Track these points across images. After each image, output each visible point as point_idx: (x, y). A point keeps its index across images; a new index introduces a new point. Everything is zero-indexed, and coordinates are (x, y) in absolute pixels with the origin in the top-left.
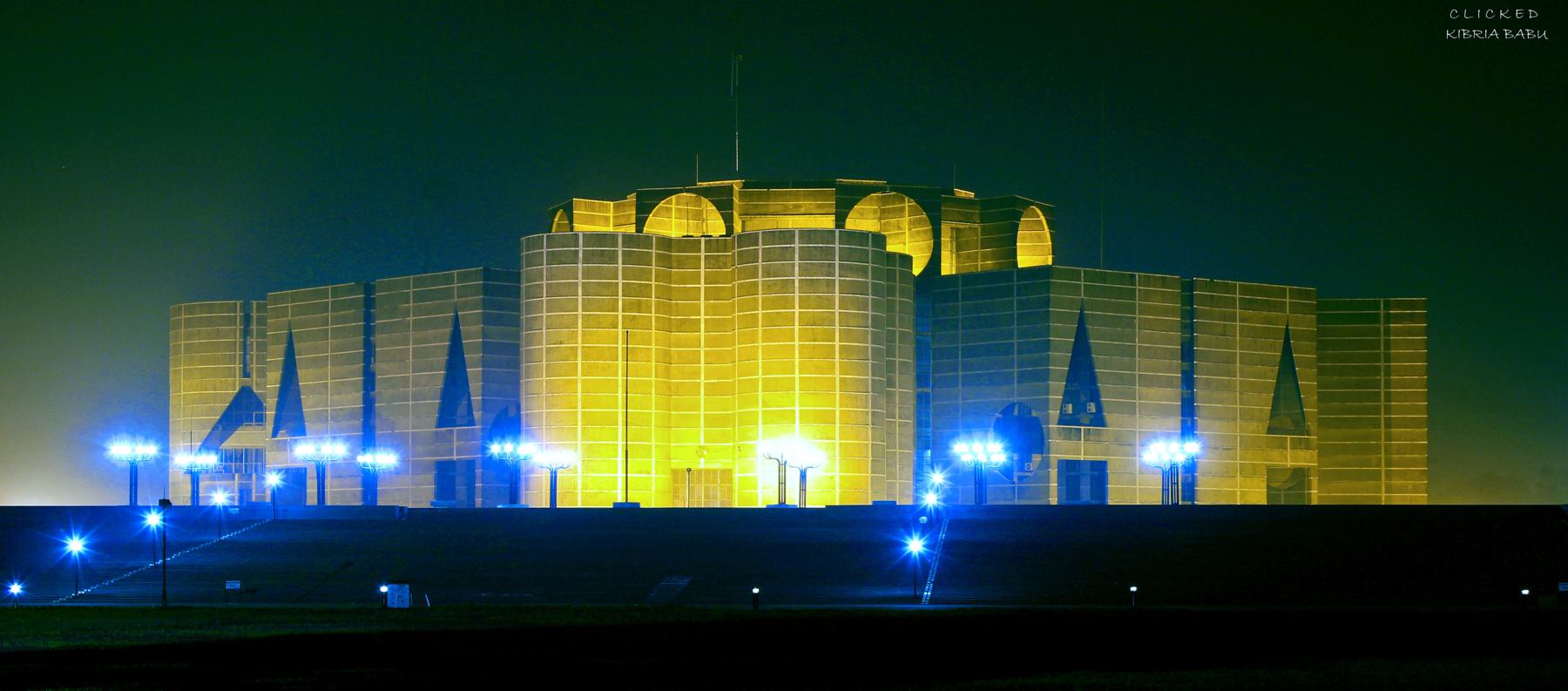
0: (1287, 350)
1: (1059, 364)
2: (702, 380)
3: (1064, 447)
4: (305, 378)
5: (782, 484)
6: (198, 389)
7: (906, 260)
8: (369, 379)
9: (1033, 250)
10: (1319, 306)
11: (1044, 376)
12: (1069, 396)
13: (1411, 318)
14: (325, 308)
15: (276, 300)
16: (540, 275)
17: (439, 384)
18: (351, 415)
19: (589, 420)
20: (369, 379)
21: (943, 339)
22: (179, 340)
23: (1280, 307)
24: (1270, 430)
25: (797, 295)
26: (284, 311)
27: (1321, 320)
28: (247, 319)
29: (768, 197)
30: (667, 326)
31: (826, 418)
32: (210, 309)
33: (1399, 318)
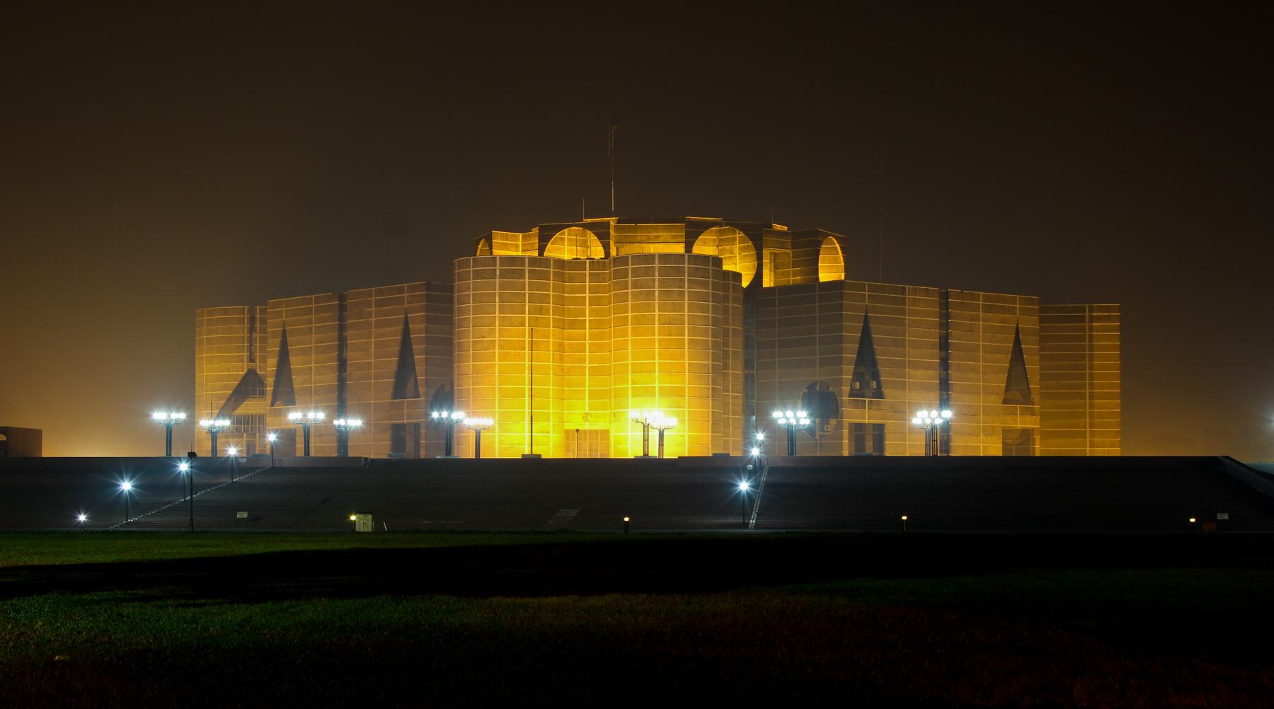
0: (1017, 342)
1: (850, 352)
2: (587, 365)
3: (854, 415)
4: (295, 363)
5: (646, 440)
6: (216, 368)
7: (737, 276)
8: (342, 364)
9: (830, 270)
11: (840, 361)
12: (857, 376)
13: (1108, 319)
16: (469, 287)
17: (394, 367)
19: (504, 395)
20: (342, 364)
21: (758, 337)
24: (1005, 402)
27: (1042, 320)
30: (561, 325)
31: (677, 393)
32: (225, 312)
33: (1100, 319)
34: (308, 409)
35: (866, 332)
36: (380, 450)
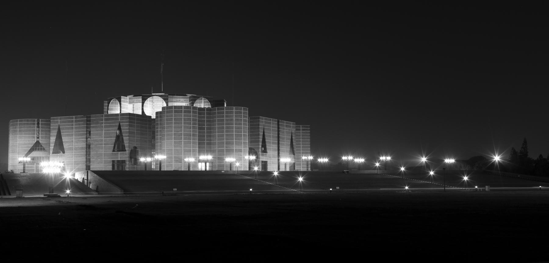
2: (206, 141)
4: (64, 139)
5: (285, 167)
10: (296, 127)
13: (307, 130)
17: (114, 141)
18: (82, 148)
22: (11, 129)
24: (64, 152)
26: (57, 122)
28: (38, 124)
29: (173, 98)
32: (28, 121)
34: (348, 156)
35: (264, 132)
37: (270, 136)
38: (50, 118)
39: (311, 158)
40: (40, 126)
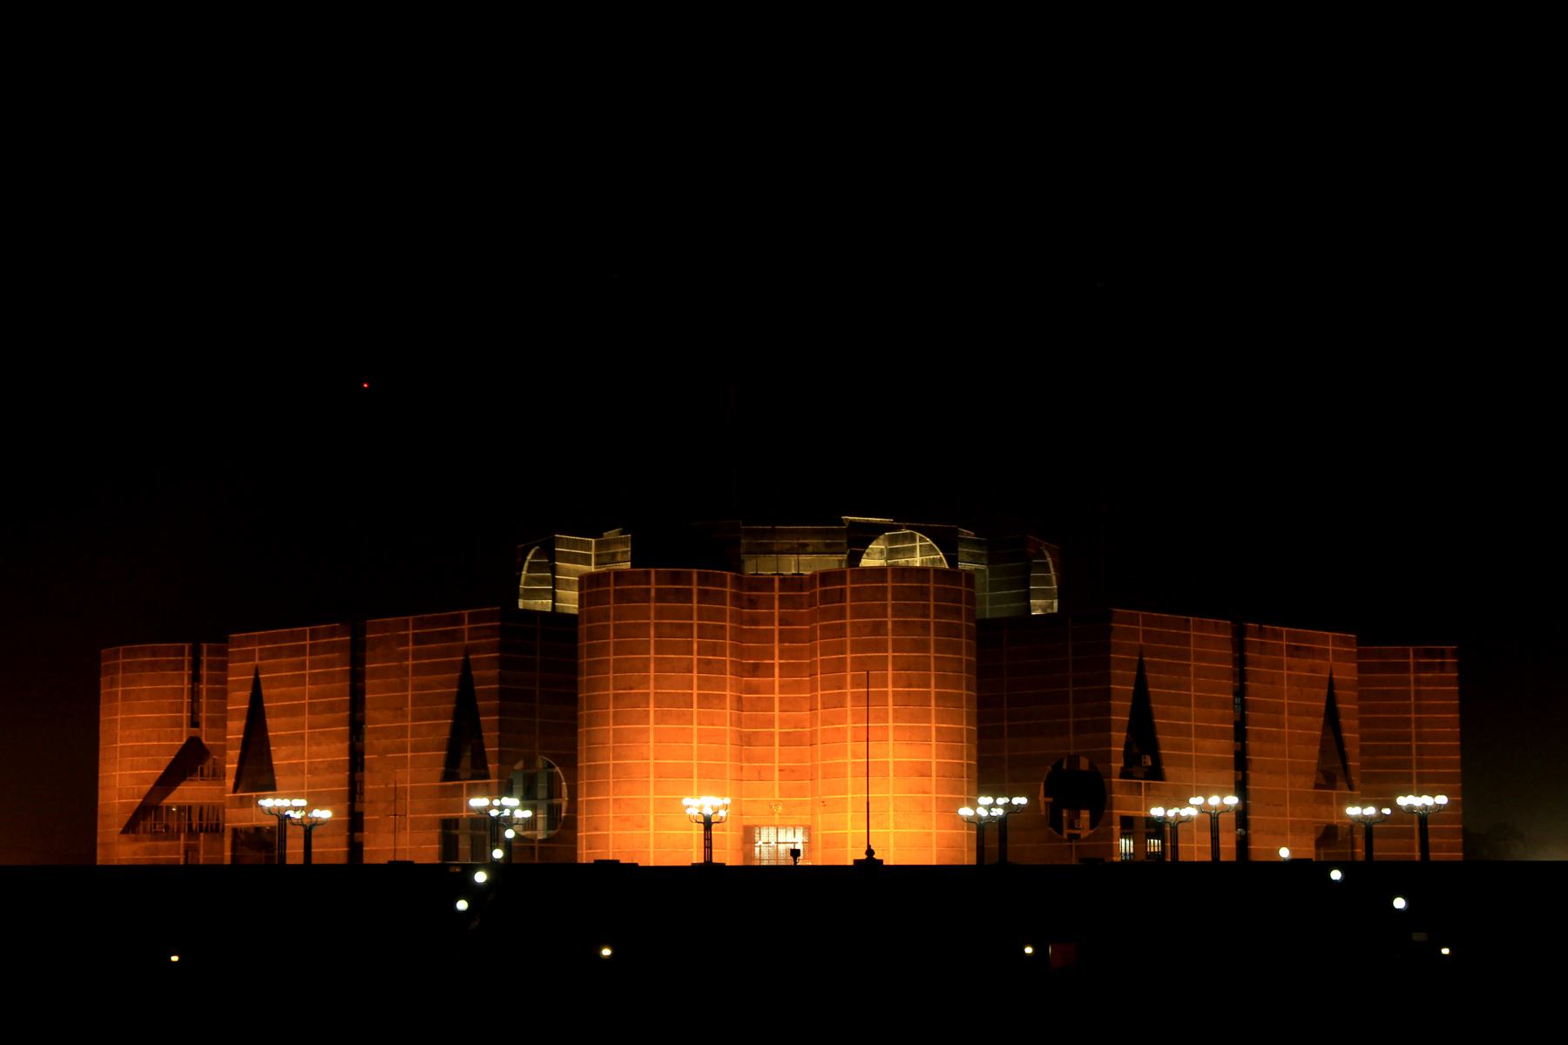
0: (1331, 700)
2: (777, 730)
4: (276, 727)
5: (1215, 840)
13: (1442, 666)
14: (300, 651)
15: (240, 643)
17: (444, 734)
18: (332, 767)
23: (1323, 654)
24: (1317, 786)
25: (890, 637)
26: (249, 656)
27: (1361, 669)
28: (196, 666)
30: (740, 670)
31: (923, 771)
36: (331, 850)
37: (294, 711)
38: (226, 641)
39: (1006, 800)
40: (204, 672)
